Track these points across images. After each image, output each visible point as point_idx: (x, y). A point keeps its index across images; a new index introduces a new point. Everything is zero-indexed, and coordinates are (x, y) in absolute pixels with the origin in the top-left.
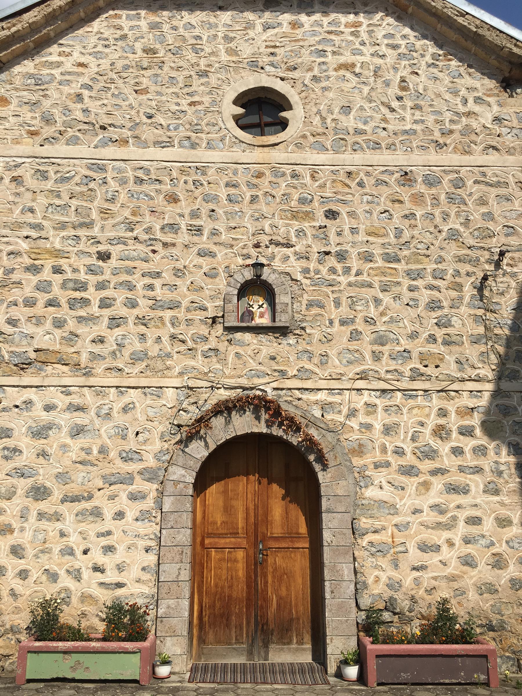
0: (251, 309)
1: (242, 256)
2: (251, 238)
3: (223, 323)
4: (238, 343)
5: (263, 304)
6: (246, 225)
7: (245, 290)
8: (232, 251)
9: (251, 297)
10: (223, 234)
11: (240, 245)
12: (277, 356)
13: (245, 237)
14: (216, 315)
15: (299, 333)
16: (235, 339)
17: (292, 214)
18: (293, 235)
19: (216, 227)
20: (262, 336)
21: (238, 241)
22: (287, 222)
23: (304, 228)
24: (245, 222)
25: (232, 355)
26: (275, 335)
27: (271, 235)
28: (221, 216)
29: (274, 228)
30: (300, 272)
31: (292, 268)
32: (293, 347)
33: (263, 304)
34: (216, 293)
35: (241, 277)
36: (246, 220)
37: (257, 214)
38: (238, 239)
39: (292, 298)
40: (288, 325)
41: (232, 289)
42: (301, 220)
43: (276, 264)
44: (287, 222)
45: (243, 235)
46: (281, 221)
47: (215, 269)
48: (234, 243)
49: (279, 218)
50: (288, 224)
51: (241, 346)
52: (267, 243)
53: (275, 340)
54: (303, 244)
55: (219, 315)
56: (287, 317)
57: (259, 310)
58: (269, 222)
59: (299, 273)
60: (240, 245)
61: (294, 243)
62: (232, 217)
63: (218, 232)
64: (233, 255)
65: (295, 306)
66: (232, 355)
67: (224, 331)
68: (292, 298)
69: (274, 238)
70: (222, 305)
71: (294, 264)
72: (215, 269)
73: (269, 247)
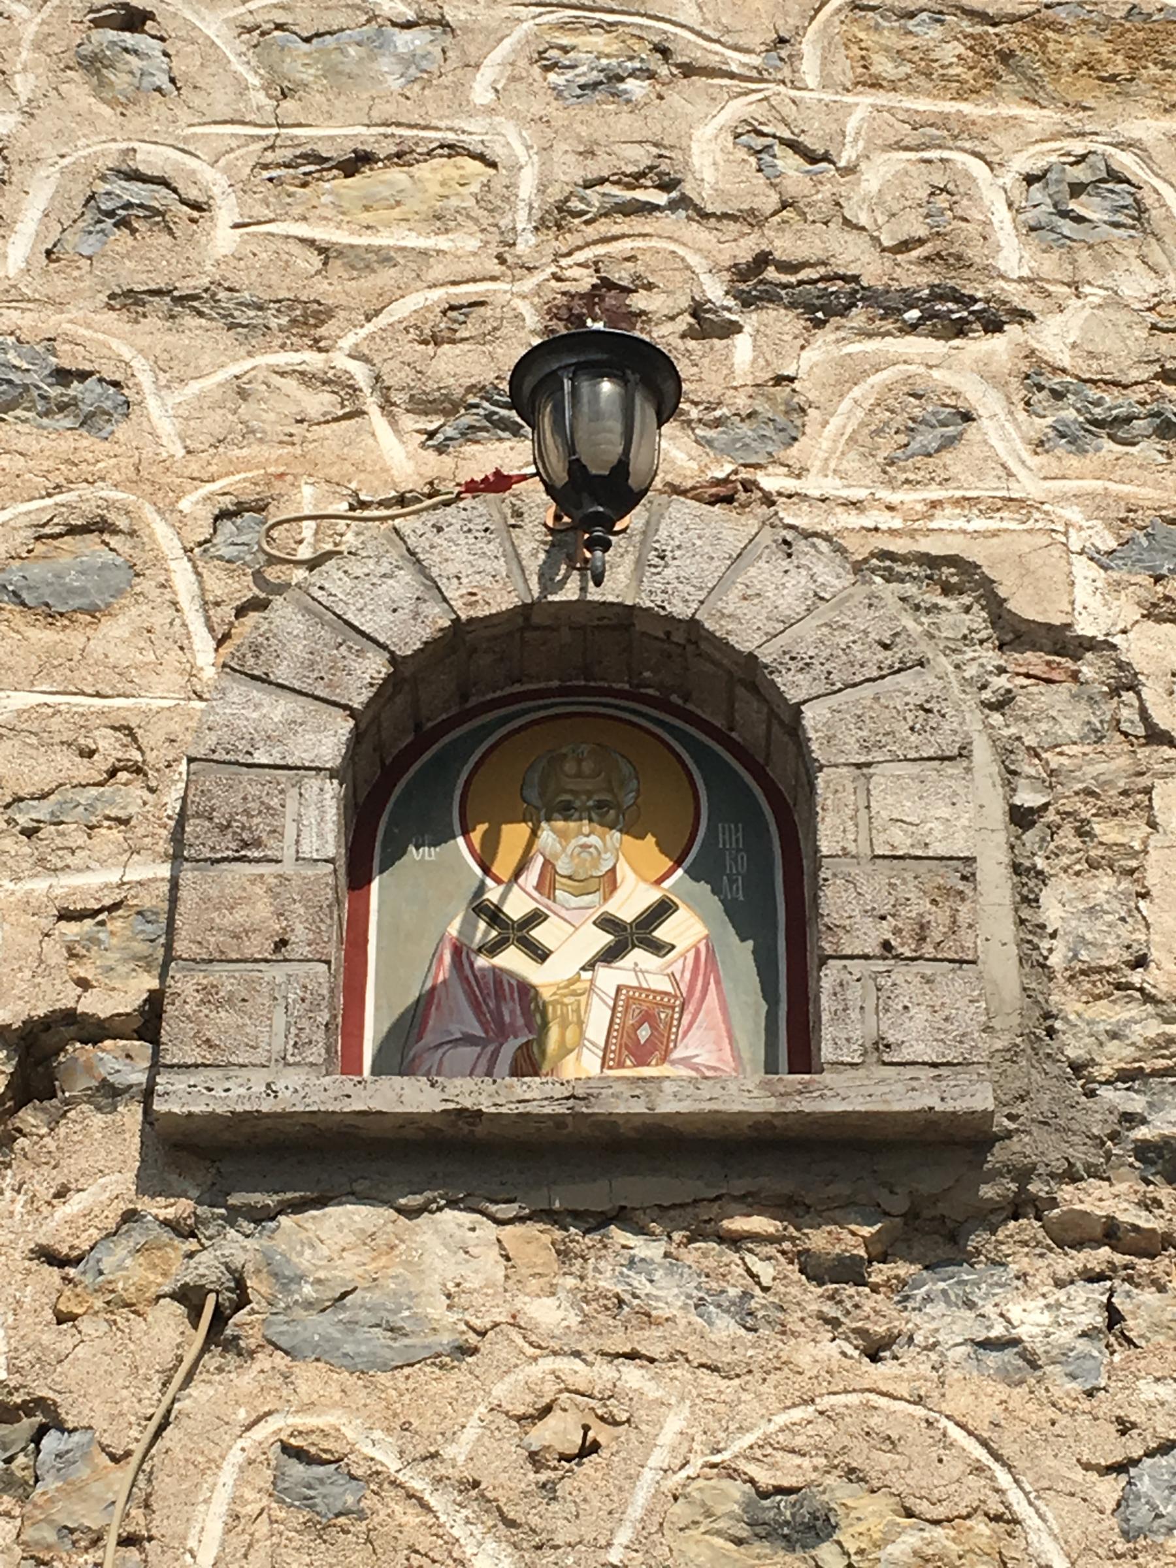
0: (512, 959)
1: (422, 405)
2: (526, 244)
3: (148, 1094)
4: (319, 1326)
5: (662, 910)
6: (475, 130)
7: (446, 764)
8: (313, 360)
9: (514, 835)
10: (226, 211)
11: (402, 309)
12: (839, 1492)
13: (466, 241)
14: (68, 997)
15: (1130, 1215)
16: (287, 1281)
17: (978, 45)
18: (1002, 216)
19: (151, 158)
20: (647, 1249)
21: (386, 277)
22: (923, 104)
23: (1125, 161)
24: (464, 107)
25: (228, 1474)
26: (818, 1240)
27: (752, 219)
28: (209, 51)
29: (789, 163)
30: (1102, 560)
31: (1008, 521)
32: (1065, 1388)
33: (662, 910)
34: (85, 771)
35: (404, 584)
36: (481, 94)
37: (598, 41)
38: (385, 258)
39: (1021, 818)
40: (981, 1099)
41: (279, 708)
42: (1086, 90)
43: (812, 485)
44: (923, 104)
45: (439, 220)
46: (866, 100)
47: (99, 527)
48: (326, 289)
49: (843, 70)
50: (942, 122)
51: (361, 1367)
52: (715, 291)
53: (813, 1297)
54: (1115, 300)
55: (97, 1005)
56: (969, 1017)
57: (609, 978)
58: (738, 109)
59: (1083, 569)
60: (402, 309)
61: (1016, 295)
62: (332, 72)
63: (159, 197)
64: (320, 402)
65: (1052, 912)
66: (228, 1474)
67: (148, 1184)
68: (1021, 818)
69: (784, 246)
70: (154, 899)
71: (1028, 486)
72: (99, 527)
73: (731, 329)
